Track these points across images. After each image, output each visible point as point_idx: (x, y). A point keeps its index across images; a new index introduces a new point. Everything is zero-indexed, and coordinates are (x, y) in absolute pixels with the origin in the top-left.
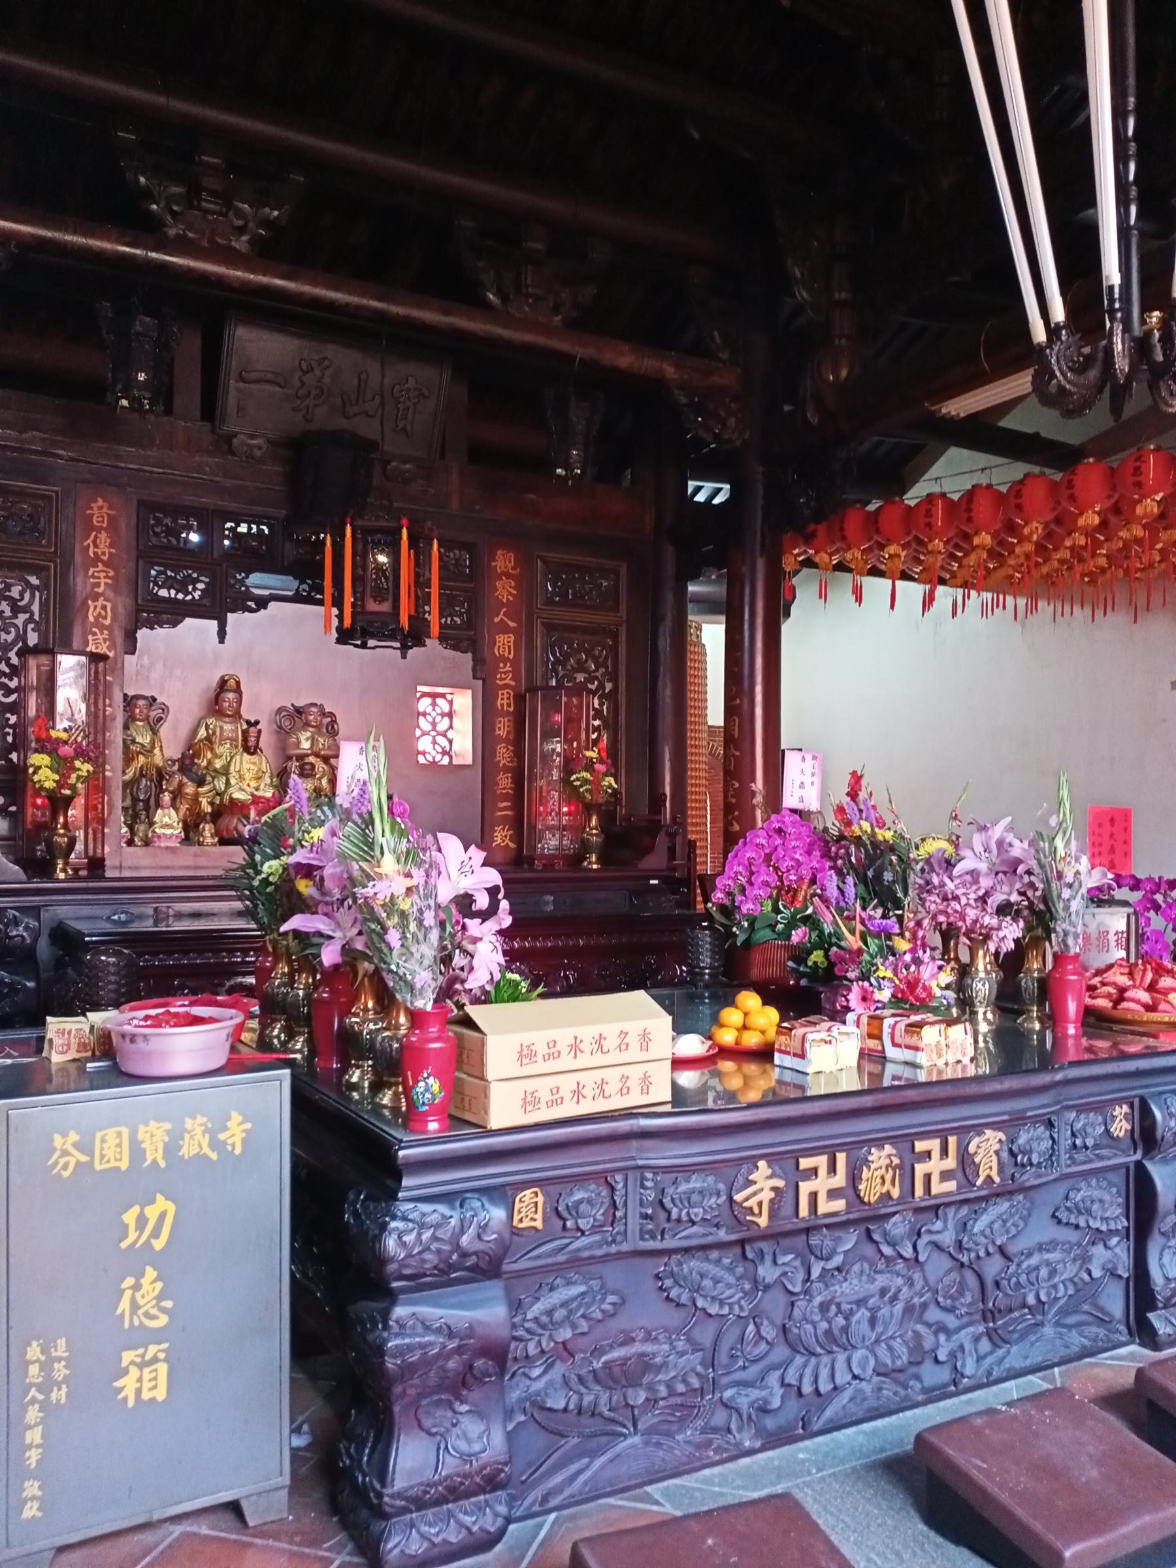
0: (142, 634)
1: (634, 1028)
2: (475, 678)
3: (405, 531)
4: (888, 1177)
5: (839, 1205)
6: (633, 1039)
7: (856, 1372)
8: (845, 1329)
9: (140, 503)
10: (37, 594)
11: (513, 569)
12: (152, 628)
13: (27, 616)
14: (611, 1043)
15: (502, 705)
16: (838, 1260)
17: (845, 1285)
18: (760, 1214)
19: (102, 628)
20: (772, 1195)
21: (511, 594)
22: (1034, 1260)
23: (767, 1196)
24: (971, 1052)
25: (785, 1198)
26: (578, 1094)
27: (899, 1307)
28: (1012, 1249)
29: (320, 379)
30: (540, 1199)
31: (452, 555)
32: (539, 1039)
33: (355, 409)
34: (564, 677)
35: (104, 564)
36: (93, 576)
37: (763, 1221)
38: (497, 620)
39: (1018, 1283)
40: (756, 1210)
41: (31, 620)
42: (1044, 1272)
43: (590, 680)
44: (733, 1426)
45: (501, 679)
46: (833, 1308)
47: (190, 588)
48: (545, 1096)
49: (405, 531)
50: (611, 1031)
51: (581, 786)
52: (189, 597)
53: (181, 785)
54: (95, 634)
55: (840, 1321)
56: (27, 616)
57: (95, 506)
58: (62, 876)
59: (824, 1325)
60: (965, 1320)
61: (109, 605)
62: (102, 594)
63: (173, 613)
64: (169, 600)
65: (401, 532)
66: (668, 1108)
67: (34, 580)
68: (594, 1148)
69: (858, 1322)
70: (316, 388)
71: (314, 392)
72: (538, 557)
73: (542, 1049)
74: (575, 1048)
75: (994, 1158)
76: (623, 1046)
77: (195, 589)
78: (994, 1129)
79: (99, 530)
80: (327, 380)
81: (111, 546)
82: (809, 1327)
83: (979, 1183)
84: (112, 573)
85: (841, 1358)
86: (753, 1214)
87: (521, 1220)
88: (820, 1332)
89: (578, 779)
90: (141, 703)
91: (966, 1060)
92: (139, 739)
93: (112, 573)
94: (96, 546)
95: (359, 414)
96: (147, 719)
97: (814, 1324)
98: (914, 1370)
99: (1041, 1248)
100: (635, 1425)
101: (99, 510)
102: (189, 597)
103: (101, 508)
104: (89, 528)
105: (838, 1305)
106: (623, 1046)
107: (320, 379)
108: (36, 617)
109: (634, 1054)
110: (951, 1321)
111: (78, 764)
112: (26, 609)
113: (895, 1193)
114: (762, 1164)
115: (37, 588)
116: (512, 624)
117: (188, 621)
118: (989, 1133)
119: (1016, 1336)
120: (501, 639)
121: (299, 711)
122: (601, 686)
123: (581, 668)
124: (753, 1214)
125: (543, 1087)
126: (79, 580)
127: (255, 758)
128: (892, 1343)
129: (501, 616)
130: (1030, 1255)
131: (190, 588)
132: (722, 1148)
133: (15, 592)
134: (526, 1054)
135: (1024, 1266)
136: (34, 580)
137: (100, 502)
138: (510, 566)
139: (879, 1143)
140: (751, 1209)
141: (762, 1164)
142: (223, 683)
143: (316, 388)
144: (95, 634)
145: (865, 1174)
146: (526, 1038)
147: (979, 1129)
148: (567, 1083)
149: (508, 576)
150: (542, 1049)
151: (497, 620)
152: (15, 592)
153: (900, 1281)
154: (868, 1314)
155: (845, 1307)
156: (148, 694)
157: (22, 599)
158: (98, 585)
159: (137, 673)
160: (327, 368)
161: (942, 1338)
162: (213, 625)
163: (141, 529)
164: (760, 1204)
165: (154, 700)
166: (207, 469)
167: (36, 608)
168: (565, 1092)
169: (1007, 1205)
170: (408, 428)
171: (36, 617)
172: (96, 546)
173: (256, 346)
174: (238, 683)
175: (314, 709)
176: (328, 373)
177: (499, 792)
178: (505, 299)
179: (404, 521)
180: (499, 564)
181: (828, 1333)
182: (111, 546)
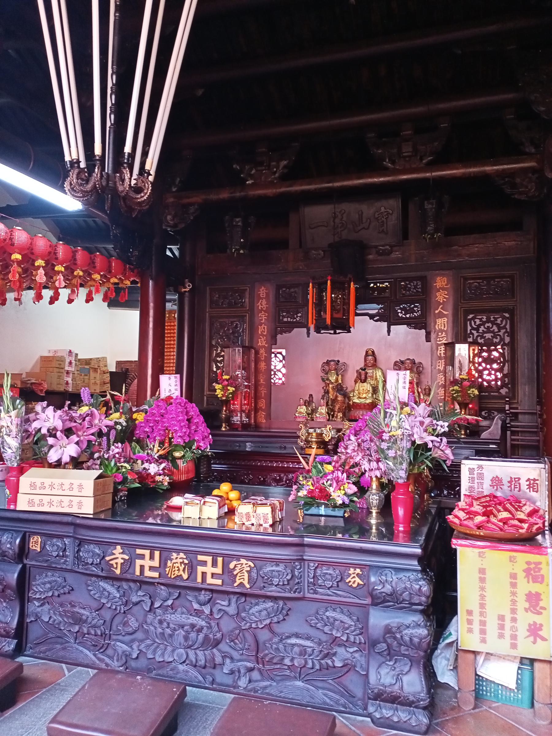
0: (279, 336)
1: (76, 482)
2: (427, 341)
3: (329, 282)
4: (181, 569)
5: (156, 574)
6: (75, 487)
7: (176, 658)
8: (171, 636)
9: (277, 285)
10: (508, 321)
11: (446, 285)
12: (282, 334)
13: (504, 330)
14: (66, 487)
15: (440, 354)
16: (170, 602)
17: (173, 615)
18: (116, 568)
19: (263, 335)
20: (123, 561)
21: (445, 298)
22: (293, 641)
23: (120, 561)
24: (271, 522)
25: (129, 564)
26: (51, 503)
27: (201, 636)
28: (278, 629)
29: (341, 219)
30: (40, 540)
31: (412, 284)
32: (38, 481)
33: (359, 228)
34: (477, 336)
35: (265, 311)
36: (261, 317)
37: (118, 572)
38: (437, 312)
39: (277, 649)
40: (115, 566)
41: (506, 332)
42: (296, 649)
43: (495, 337)
44: (115, 658)
45: (440, 341)
46: (165, 624)
47: (295, 316)
48: (37, 502)
49: (329, 282)
50: (76, 482)
51: (455, 393)
52: (295, 320)
53: (337, 397)
54: (261, 338)
55: (168, 631)
56: (504, 330)
57: (261, 290)
58: (224, 429)
59: (160, 630)
60: (244, 657)
61: (266, 327)
62: (263, 323)
63: (289, 327)
64: (288, 322)
65: (327, 282)
66: (91, 516)
67: (507, 315)
68: (58, 526)
69: (178, 635)
70: (340, 223)
71: (340, 225)
72: (461, 277)
73: (38, 485)
74: (52, 486)
75: (246, 575)
76: (71, 489)
77: (297, 316)
78: (247, 560)
79: (262, 299)
80: (345, 219)
81: (266, 304)
82: (152, 628)
83: (235, 585)
84: (267, 315)
85: (169, 649)
86: (113, 567)
87: (32, 546)
88: (158, 633)
89: (453, 390)
90: (332, 363)
91: (267, 525)
92: (330, 378)
93: (267, 315)
94: (262, 305)
95: (362, 229)
96: (335, 369)
97: (155, 628)
98: (212, 671)
99: (297, 636)
100: (76, 640)
101: (262, 291)
102: (295, 320)
103: (263, 290)
104: (260, 298)
105: (168, 624)
106: (71, 489)
107: (341, 219)
108: (508, 330)
109: (75, 492)
110: (236, 655)
111: (229, 388)
112: (504, 327)
113: (185, 576)
114: (119, 547)
115: (508, 318)
116: (445, 313)
117: (295, 329)
118: (243, 561)
119: (279, 678)
120: (439, 321)
121: (402, 362)
122: (502, 339)
123: (488, 330)
124: (113, 567)
125: (37, 498)
126: (256, 318)
127: (365, 384)
128: (198, 652)
129: (439, 309)
130: (288, 637)
131: (295, 316)
132: (125, 538)
133: (499, 321)
134: (33, 486)
135: (284, 642)
136: (507, 315)
137: (263, 288)
138: (444, 284)
139: (178, 551)
140: (112, 564)
141: (119, 547)
142: (367, 355)
143: (340, 223)
144: (261, 338)
145: (169, 564)
146: (33, 480)
147: (238, 558)
148: (46, 499)
149: (443, 289)
150: (38, 485)
151: (437, 312)
152: (499, 321)
153: (204, 623)
154: (183, 633)
155: (172, 626)
156: (336, 359)
157: (502, 324)
158: (262, 320)
159: (339, 351)
160: (343, 214)
161: (228, 661)
162: (305, 330)
163: (277, 296)
164: (117, 563)
165: (338, 361)
166: (301, 267)
167: (508, 327)
168: (45, 502)
169: (272, 604)
170: (385, 230)
171: (508, 330)
172: (262, 305)
173: (320, 212)
174: (373, 352)
175: (408, 361)
176: (345, 215)
177: (439, 398)
178: (393, 162)
179: (329, 278)
180: (438, 284)
181: (163, 634)
182: (266, 304)
